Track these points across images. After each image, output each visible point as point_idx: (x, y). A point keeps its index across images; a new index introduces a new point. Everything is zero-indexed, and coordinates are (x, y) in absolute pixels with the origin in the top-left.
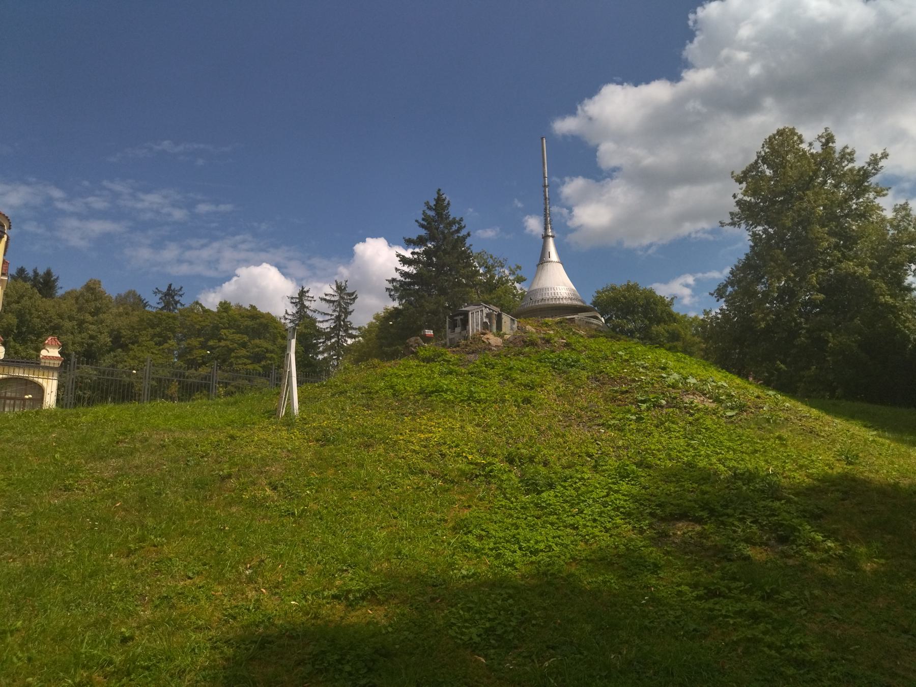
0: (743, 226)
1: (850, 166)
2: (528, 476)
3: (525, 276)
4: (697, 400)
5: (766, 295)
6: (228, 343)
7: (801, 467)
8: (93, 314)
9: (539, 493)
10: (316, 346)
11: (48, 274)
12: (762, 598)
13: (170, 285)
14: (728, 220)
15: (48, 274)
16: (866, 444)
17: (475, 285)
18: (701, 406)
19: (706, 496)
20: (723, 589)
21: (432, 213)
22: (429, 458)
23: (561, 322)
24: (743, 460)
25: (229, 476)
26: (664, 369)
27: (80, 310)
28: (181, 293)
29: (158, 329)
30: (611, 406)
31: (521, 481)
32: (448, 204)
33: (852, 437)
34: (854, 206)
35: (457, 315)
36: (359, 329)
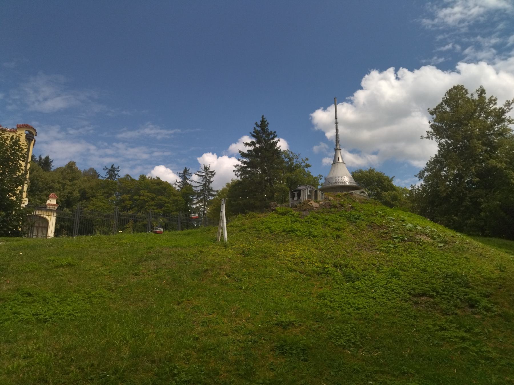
0: (434, 139)
1: (494, 106)
2: (347, 274)
3: (311, 164)
4: (423, 238)
5: (446, 177)
6: (145, 197)
7: (478, 272)
8: (70, 181)
9: (353, 282)
10: (192, 200)
11: (47, 158)
12: (466, 332)
13: (113, 165)
14: (425, 135)
15: (47, 158)
16: (509, 262)
17: (282, 169)
18: (425, 241)
19: (435, 286)
20: (447, 327)
21: (259, 129)
22: (296, 264)
23: (346, 195)
24: (449, 268)
25: (207, 270)
26: (403, 221)
27: (64, 178)
28: (118, 170)
29: (107, 190)
30: (380, 240)
31: (343, 276)
32: (268, 123)
33: (502, 258)
34: (496, 129)
35: (296, 191)
36: (217, 191)
